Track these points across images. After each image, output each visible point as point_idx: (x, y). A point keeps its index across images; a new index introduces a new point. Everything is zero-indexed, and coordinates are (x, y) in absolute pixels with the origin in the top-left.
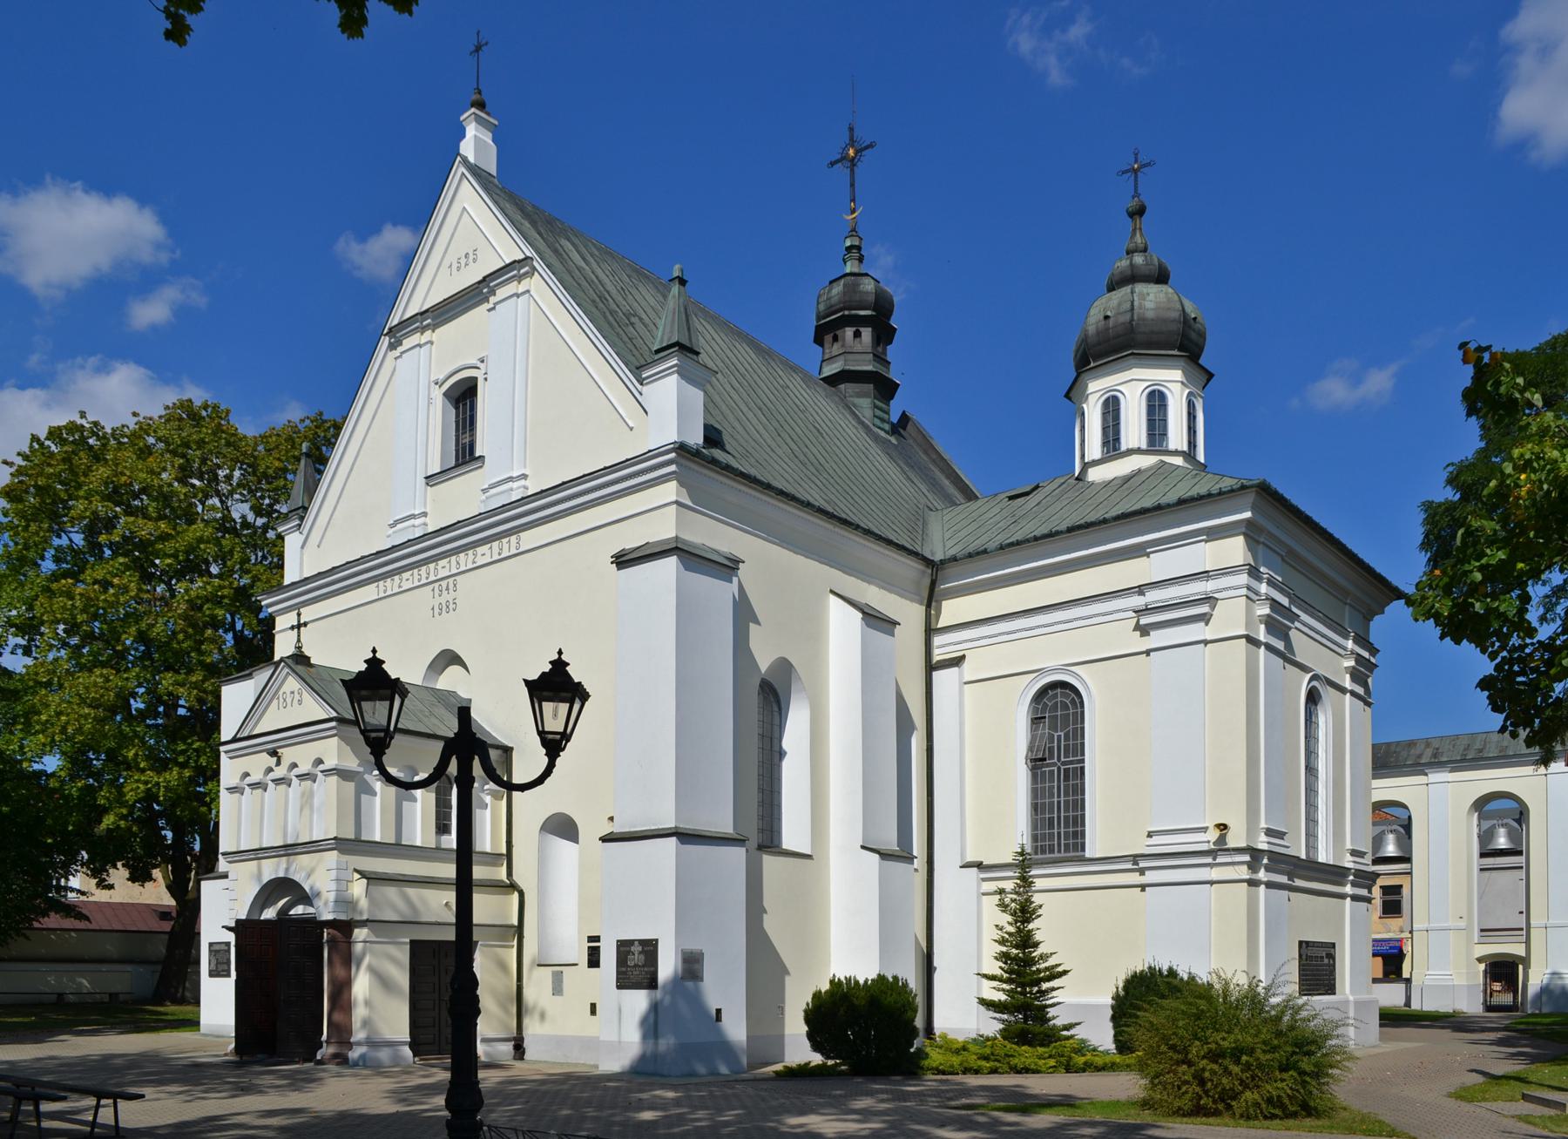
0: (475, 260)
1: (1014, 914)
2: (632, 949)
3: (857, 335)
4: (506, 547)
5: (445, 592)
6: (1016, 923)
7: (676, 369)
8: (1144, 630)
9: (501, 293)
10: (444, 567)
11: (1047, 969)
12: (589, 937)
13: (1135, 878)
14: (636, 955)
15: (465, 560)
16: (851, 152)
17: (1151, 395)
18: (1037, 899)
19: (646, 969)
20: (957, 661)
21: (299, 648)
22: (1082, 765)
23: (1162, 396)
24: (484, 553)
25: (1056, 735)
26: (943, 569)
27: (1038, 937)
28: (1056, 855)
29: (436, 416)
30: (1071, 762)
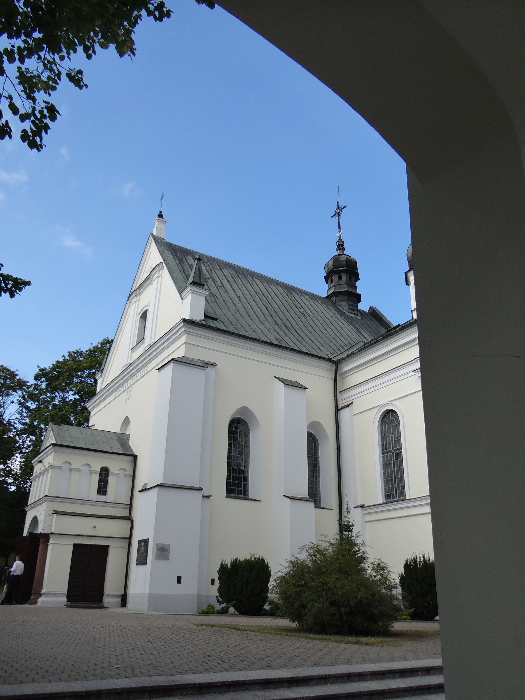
3: (340, 278)
22: (401, 451)
25: (391, 436)
26: (340, 364)
28: (395, 499)
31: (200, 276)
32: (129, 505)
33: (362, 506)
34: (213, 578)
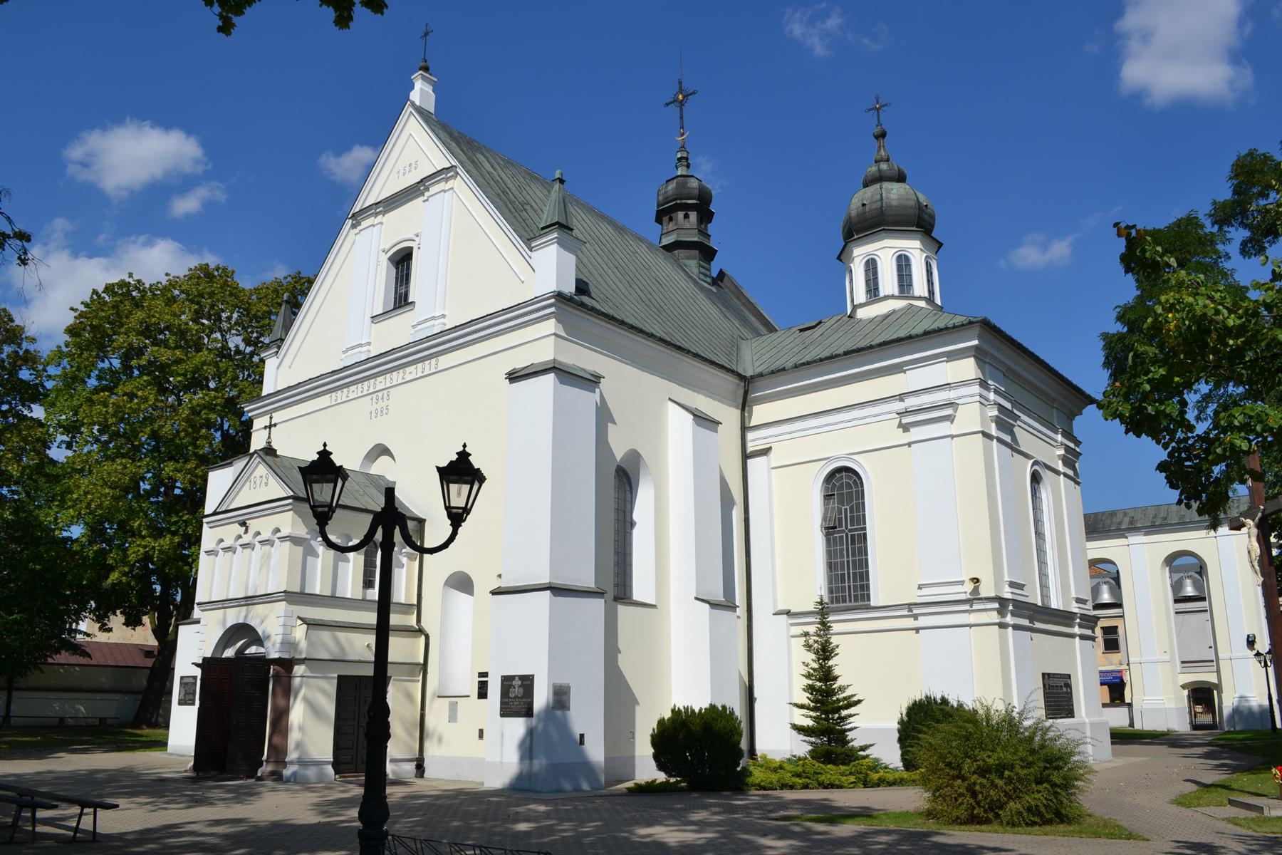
0: (416, 168)
1: (816, 653)
2: (514, 683)
3: (686, 216)
6: (819, 661)
7: (556, 240)
8: (905, 428)
9: (433, 190)
10: (381, 382)
11: (845, 699)
12: (479, 673)
13: (910, 623)
14: (517, 688)
15: (396, 377)
16: (680, 97)
17: (899, 257)
18: (835, 640)
19: (524, 700)
20: (765, 452)
21: (269, 443)
23: (907, 258)
24: (411, 372)
27: (836, 672)
28: (848, 604)
29: (383, 273)
30: (856, 530)
33: (788, 613)
34: (481, 728)
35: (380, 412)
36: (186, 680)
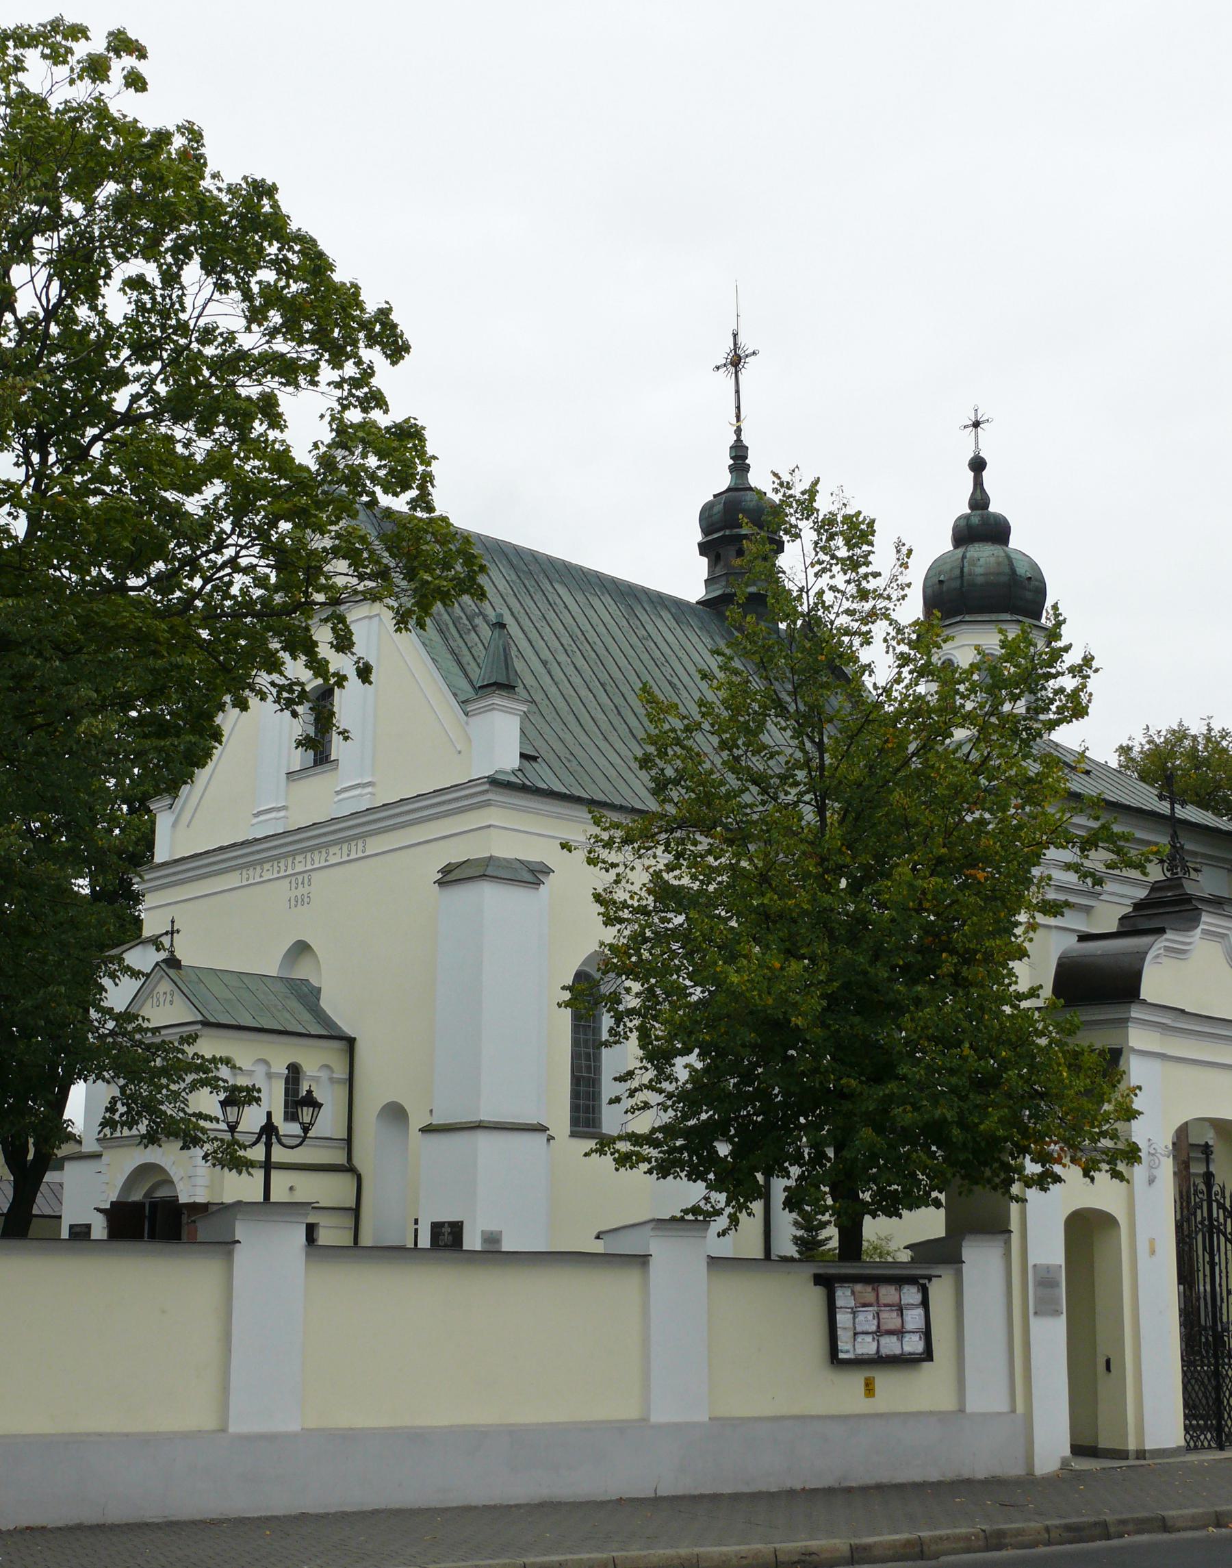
2: (443, 1230)
4: (354, 849)
5: (300, 886)
15: (319, 860)
23: (447, 870)
31: (507, 669)
32: (844, 1297)
35: (300, 900)
36: (78, 1230)
